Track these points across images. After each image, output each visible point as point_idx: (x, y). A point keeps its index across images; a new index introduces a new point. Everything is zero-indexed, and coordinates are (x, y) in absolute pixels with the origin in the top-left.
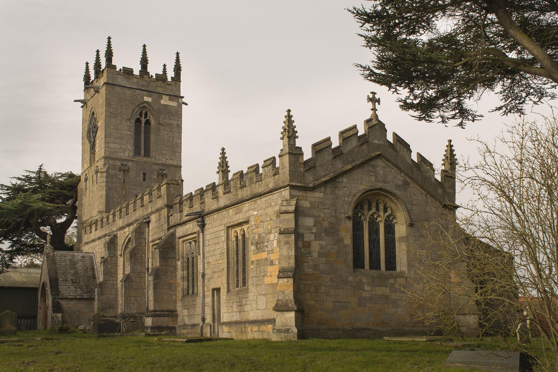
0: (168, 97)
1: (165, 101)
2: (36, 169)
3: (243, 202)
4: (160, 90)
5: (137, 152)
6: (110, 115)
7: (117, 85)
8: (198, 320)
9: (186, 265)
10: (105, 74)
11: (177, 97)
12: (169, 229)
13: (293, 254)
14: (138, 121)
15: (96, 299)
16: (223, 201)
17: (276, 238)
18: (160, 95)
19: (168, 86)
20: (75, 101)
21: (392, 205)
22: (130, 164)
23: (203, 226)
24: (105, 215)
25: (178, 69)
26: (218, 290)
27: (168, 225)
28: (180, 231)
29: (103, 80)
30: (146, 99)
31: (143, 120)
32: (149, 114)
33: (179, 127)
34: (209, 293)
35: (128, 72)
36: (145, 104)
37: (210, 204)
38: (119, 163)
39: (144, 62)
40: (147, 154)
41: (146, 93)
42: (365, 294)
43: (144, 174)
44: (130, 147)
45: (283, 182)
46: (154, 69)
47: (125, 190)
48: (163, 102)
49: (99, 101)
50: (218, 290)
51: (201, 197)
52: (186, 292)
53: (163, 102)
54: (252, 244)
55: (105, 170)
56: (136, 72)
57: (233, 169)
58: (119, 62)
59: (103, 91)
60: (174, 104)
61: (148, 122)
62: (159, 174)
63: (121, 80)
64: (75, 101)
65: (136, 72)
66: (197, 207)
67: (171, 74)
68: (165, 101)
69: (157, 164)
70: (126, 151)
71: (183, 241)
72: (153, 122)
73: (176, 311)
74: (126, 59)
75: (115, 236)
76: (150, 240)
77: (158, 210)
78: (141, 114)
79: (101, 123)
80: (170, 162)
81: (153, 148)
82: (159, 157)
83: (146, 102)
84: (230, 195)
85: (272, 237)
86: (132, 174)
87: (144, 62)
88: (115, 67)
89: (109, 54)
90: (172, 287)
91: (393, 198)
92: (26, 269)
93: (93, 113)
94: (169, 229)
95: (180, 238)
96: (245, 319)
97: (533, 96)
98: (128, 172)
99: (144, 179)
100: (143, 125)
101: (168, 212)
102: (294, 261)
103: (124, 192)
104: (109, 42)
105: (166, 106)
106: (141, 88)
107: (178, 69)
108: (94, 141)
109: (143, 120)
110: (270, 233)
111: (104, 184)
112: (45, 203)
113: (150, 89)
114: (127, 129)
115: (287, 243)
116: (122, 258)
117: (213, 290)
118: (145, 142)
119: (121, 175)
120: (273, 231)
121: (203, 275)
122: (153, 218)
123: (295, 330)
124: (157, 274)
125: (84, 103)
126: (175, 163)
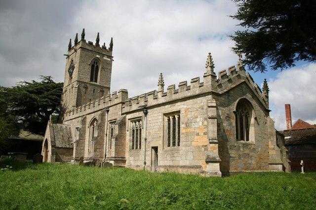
3: (181, 99)
4: (103, 53)
5: (91, 80)
6: (81, 62)
8: (141, 163)
9: (132, 133)
10: (81, 44)
11: (111, 57)
15: (75, 148)
16: (162, 100)
18: (104, 55)
19: (107, 52)
21: (248, 108)
23: (146, 114)
24: (75, 108)
25: (111, 45)
29: (78, 46)
30: (98, 56)
33: (111, 69)
35: (91, 43)
39: (98, 40)
42: (241, 153)
44: (89, 77)
46: (101, 44)
49: (76, 57)
52: (131, 148)
53: (104, 58)
57: (217, 70)
59: (79, 51)
60: (109, 60)
66: (142, 103)
67: (108, 47)
70: (87, 78)
74: (90, 38)
78: (95, 63)
79: (76, 66)
85: (198, 120)
86: (89, 89)
87: (98, 40)
88: (85, 41)
89: (83, 35)
90: (123, 145)
93: (73, 61)
96: (176, 164)
97: (72, 113)
107: (111, 45)
110: (197, 117)
114: (88, 69)
115: (212, 123)
116: (89, 129)
117: (152, 148)
120: (199, 117)
121: (146, 139)
123: (220, 173)
124: (77, 142)
125: (68, 56)
126: (108, 86)
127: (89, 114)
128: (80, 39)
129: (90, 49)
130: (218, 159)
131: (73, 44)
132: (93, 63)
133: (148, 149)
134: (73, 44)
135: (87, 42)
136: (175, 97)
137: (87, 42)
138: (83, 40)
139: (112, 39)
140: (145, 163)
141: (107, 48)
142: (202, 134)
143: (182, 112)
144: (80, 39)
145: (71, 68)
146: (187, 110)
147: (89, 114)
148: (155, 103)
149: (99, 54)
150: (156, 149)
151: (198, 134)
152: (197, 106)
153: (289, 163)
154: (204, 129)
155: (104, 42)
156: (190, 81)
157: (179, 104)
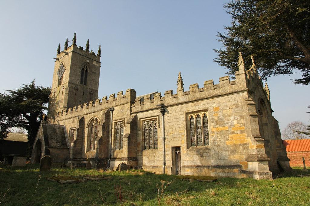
0: (95, 62)
1: (94, 63)
2: (31, 84)
5: (81, 83)
7: (77, 53)
11: (99, 62)
12: (131, 114)
13: (258, 127)
14: (83, 69)
16: (181, 99)
17: (236, 118)
19: (96, 58)
20: (54, 58)
22: (79, 87)
25: (100, 51)
26: (178, 148)
27: (131, 112)
28: (140, 116)
30: (87, 61)
31: (85, 70)
32: (88, 67)
34: (169, 153)
35: (81, 49)
36: (87, 63)
37: (168, 100)
38: (74, 86)
39: (88, 46)
40: (85, 84)
41: (87, 58)
43: (84, 92)
44: (79, 80)
45: (240, 88)
47: (76, 98)
48: (93, 63)
49: (67, 60)
50: (178, 148)
51: (71, 111)
52: (144, 148)
54: (212, 122)
55: (68, 88)
56: (85, 49)
58: (79, 44)
59: (70, 54)
60: (97, 65)
61: (87, 71)
62: (89, 93)
63: (78, 51)
64: (54, 58)
65: (85, 49)
68: (94, 63)
69: (89, 89)
70: (78, 82)
71: (143, 121)
72: (89, 71)
73: (137, 158)
75: (83, 118)
76: (113, 119)
77: (122, 104)
78: (84, 67)
80: (94, 88)
81: (88, 82)
82: (90, 86)
83: (87, 62)
84: (189, 96)
87: (88, 46)
88: (76, 45)
91: (264, 105)
92: (17, 133)
94: (131, 114)
95: (140, 119)
98: (78, 91)
99: (84, 95)
100: (85, 71)
101: (131, 105)
102: (259, 131)
103: (75, 99)
104: (75, 35)
105: (94, 65)
106: (86, 56)
107: (100, 51)
108: (62, 76)
109: (85, 70)
110: (230, 115)
111: (68, 94)
112: (30, 102)
113: (89, 57)
115: (254, 121)
116: (87, 129)
118: (85, 78)
119: (74, 91)
122: (117, 109)
126: (96, 89)
127: (88, 114)
128: (70, 44)
129: (80, 53)
130: (265, 157)
131: (63, 48)
132: (83, 67)
133: (168, 149)
134: (63, 48)
135: (78, 47)
136: (198, 95)
137: (78, 47)
138: (75, 45)
139: (100, 47)
140: (165, 164)
141: (96, 55)
142: (238, 132)
143: (211, 110)
144: (70, 44)
145: (61, 72)
146: (216, 109)
147: (88, 114)
148: (175, 101)
149: (89, 59)
150: (176, 149)
151: (233, 133)
152: (229, 104)
153: (145, 199)
154: (241, 127)
155: (94, 49)
156: (164, 93)
157: (205, 101)
